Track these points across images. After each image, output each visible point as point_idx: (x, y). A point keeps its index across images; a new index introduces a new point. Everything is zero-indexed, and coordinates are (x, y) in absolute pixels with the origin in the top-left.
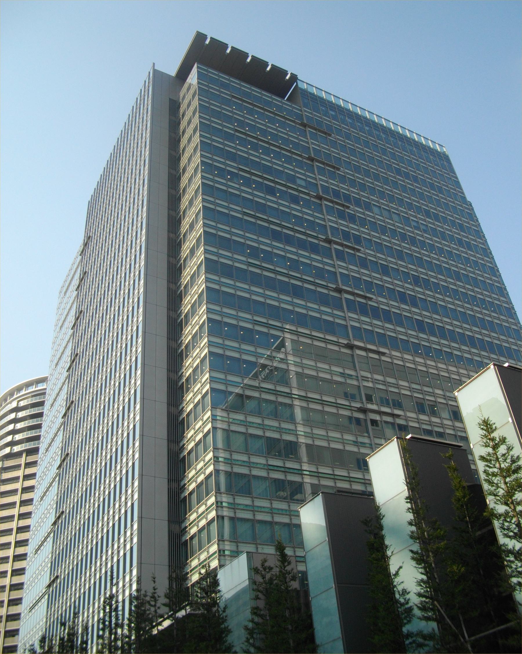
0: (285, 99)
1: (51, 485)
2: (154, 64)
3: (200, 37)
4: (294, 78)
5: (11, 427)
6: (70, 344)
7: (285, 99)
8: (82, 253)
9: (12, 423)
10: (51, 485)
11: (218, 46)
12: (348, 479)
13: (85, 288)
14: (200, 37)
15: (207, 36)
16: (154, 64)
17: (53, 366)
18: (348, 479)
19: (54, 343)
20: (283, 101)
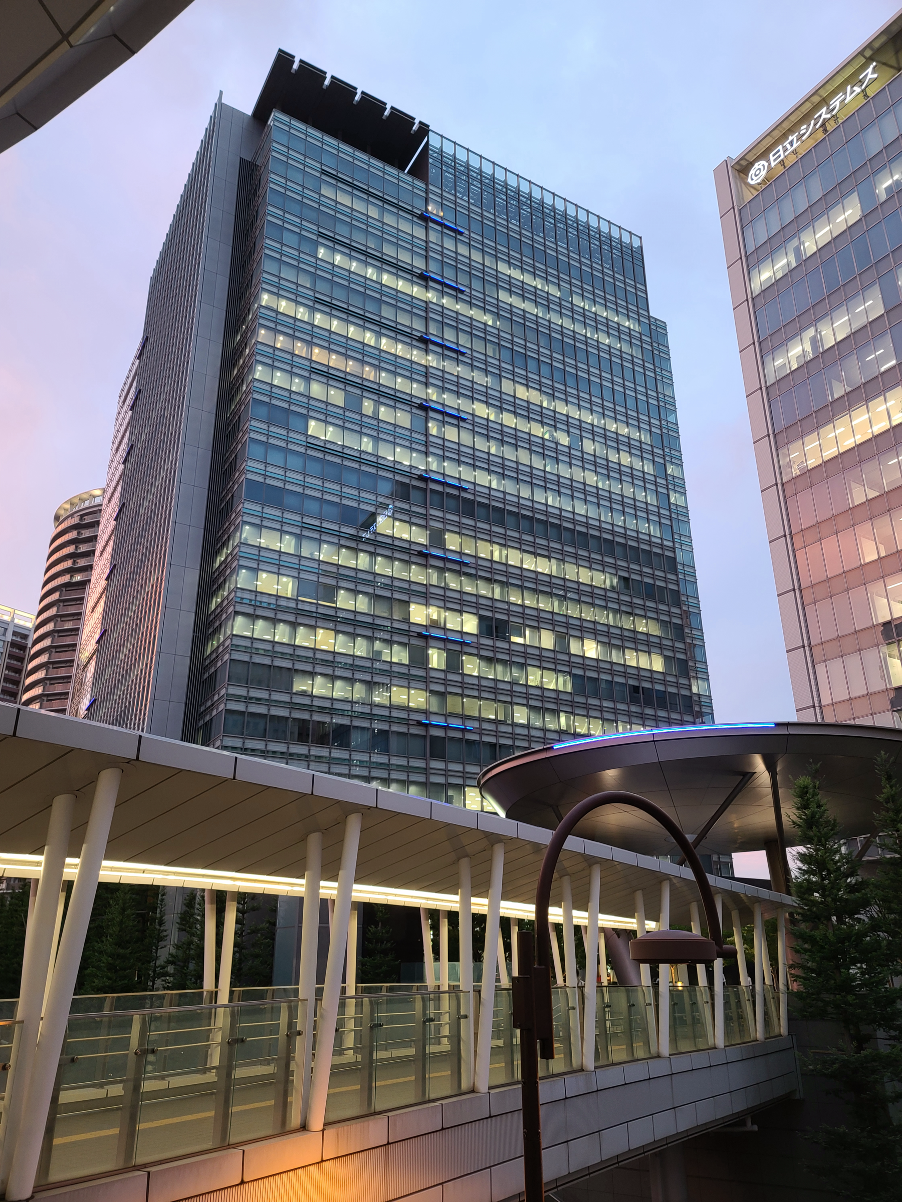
0: (406, 171)
1: (98, 602)
2: (221, 92)
3: (283, 60)
4: (424, 129)
5: (68, 564)
6: (102, 601)
7: (406, 171)
8: (140, 357)
9: (76, 529)
10: (98, 602)
11: (312, 74)
12: (318, 529)
13: (124, 518)
14: (283, 60)
15: (293, 57)
16: (221, 92)
17: (121, 403)
18: (318, 529)
19: (112, 461)
20: (401, 175)
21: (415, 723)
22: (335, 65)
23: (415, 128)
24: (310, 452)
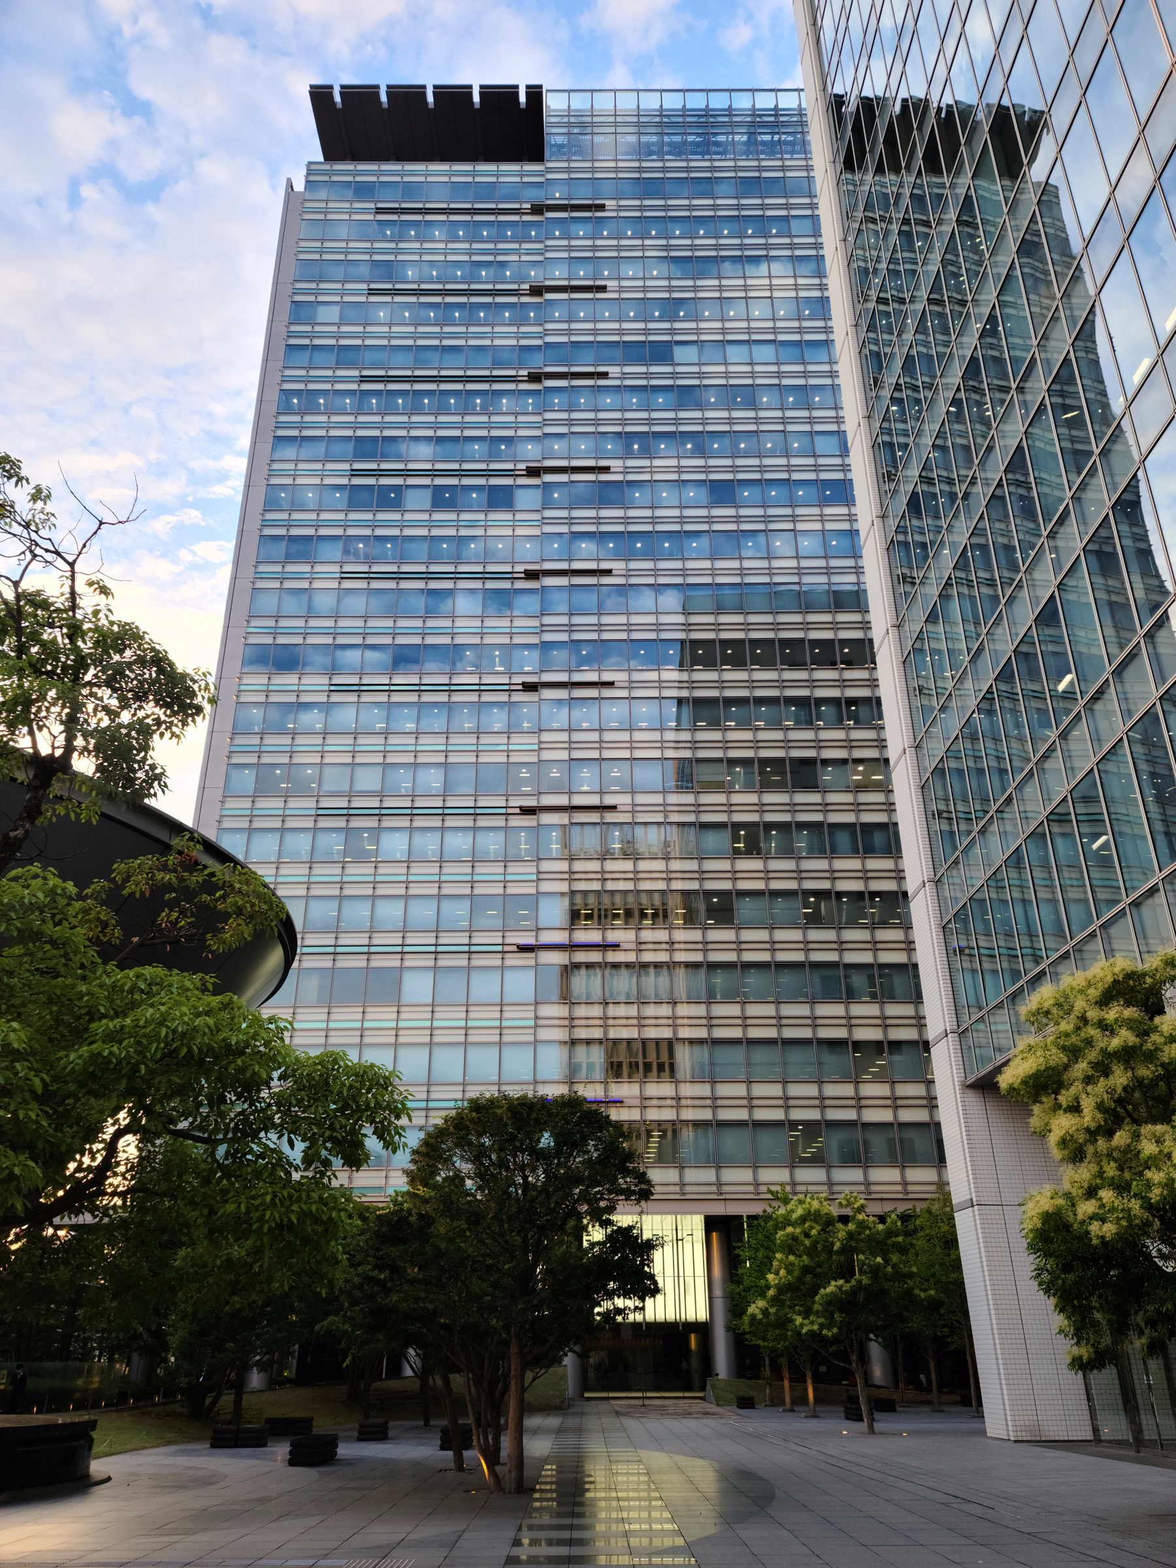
14: (320, 96)
21: (515, 948)
22: (385, 73)
23: (522, 98)
24: (347, 584)
